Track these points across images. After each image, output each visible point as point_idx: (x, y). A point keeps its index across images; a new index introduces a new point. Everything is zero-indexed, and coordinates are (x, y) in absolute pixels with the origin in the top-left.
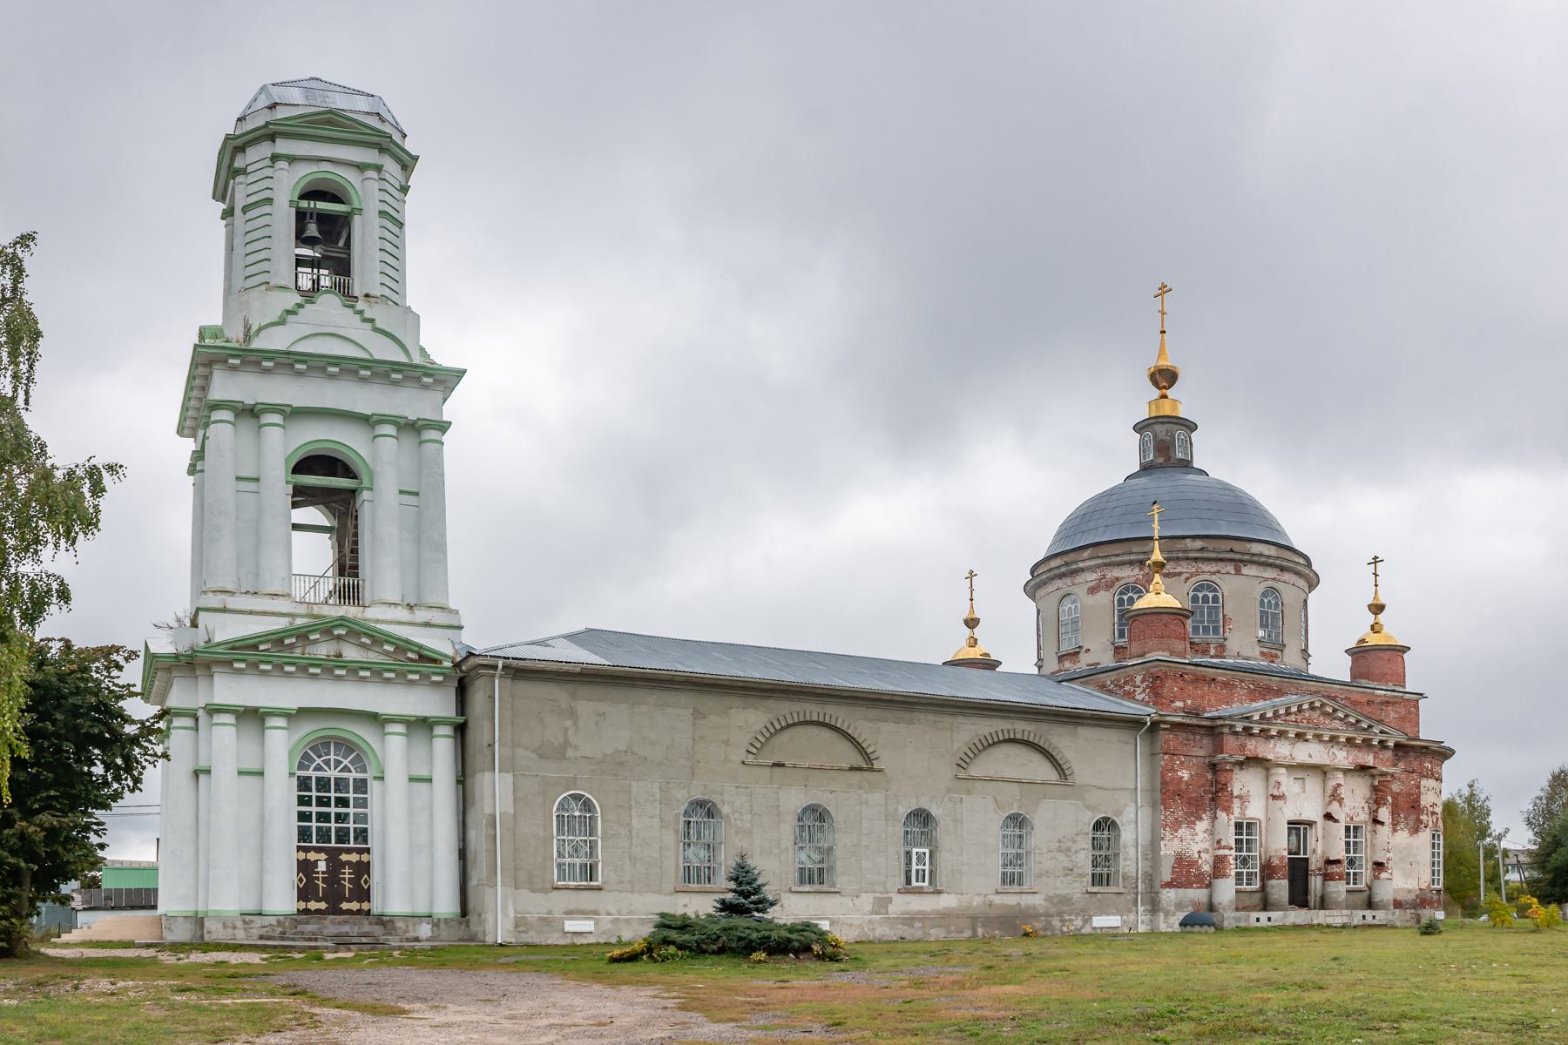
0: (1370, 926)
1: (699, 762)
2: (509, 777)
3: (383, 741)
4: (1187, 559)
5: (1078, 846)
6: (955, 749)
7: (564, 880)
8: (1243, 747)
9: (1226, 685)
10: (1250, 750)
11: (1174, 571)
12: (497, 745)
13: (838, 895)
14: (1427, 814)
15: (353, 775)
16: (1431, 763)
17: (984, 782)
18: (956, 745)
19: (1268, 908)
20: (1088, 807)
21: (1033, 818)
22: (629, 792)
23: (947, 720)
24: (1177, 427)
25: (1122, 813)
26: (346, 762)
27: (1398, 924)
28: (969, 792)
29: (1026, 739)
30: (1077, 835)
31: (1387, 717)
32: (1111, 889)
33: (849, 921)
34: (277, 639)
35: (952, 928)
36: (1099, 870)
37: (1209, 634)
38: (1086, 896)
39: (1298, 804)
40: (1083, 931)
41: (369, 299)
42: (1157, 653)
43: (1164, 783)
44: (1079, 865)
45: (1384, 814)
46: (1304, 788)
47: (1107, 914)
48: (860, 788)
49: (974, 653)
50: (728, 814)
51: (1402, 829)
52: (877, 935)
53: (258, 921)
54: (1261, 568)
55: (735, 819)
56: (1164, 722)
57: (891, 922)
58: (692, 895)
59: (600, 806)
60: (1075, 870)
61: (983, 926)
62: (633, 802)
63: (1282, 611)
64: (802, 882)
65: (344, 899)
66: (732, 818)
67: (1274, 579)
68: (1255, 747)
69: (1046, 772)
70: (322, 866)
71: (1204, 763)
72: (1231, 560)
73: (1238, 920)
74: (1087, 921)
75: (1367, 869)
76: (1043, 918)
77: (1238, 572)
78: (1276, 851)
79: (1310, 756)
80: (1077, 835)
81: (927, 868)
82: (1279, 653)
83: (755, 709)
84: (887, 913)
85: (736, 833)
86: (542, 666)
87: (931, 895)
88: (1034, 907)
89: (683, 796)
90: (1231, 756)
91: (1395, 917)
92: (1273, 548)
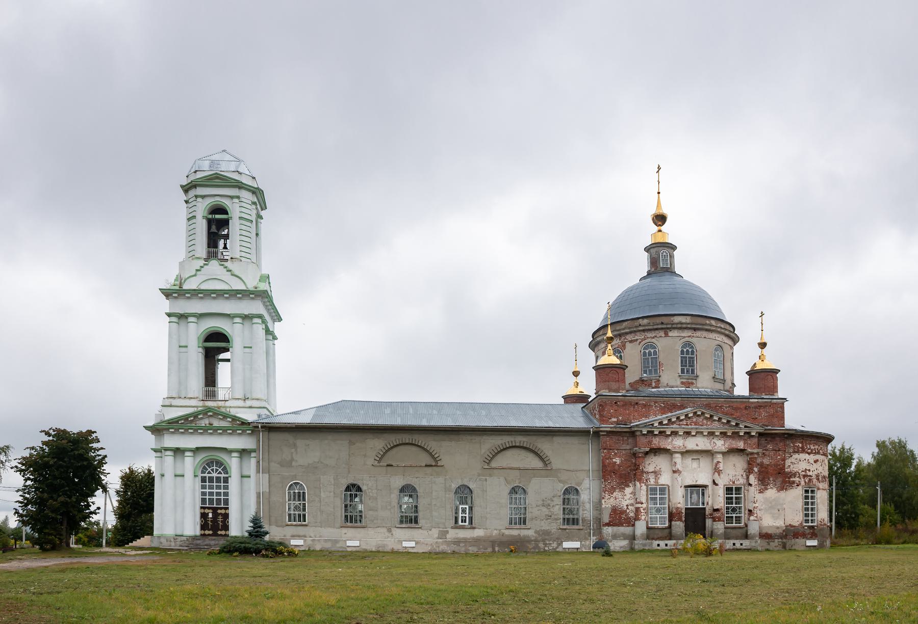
0: (738, 550)
1: (351, 465)
2: (267, 476)
3: (231, 460)
4: (640, 331)
5: (555, 503)
6: (482, 453)
7: (300, 521)
8: (650, 442)
9: (644, 406)
10: (655, 444)
11: (634, 339)
12: (261, 461)
13: (420, 529)
14: (799, 477)
15: (223, 475)
16: (802, 443)
17: (499, 470)
18: (483, 451)
19: (672, 538)
20: (560, 481)
21: (528, 488)
22: (320, 481)
23: (477, 438)
24: (661, 248)
25: (582, 483)
26: (220, 470)
27: (759, 548)
28: (490, 476)
29: (522, 445)
30: (553, 497)
31: (760, 415)
32: (576, 527)
33: (426, 542)
34: (186, 418)
35: (481, 547)
36: (567, 516)
37: (684, 355)
38: (560, 530)
39: (695, 475)
40: (558, 550)
41: (232, 260)
42: (604, 390)
43: (604, 466)
44: (555, 513)
45: (753, 479)
46: (699, 464)
47: (572, 541)
48: (431, 475)
49: (576, 391)
50: (365, 490)
51: (771, 488)
52: (440, 549)
53: (180, 539)
54: (681, 331)
55: (369, 492)
56: (601, 431)
57: (448, 543)
58: (349, 529)
59: (307, 487)
60: (553, 516)
61: (499, 546)
62: (321, 485)
63: (696, 355)
64: (401, 522)
65: (219, 530)
66: (367, 491)
67: (690, 336)
68: (657, 442)
69: (536, 463)
70: (210, 515)
71: (630, 453)
72: (662, 329)
73: (645, 545)
74: (560, 544)
75: (745, 514)
76: (533, 542)
77: (666, 335)
78: (674, 504)
79: (697, 445)
80: (553, 497)
81: (467, 515)
82: (694, 381)
83: (378, 439)
84: (446, 538)
85: (369, 499)
86: (278, 425)
87: (470, 530)
88: (528, 537)
89: (345, 483)
90: (640, 448)
91: (757, 544)
92: (689, 318)
